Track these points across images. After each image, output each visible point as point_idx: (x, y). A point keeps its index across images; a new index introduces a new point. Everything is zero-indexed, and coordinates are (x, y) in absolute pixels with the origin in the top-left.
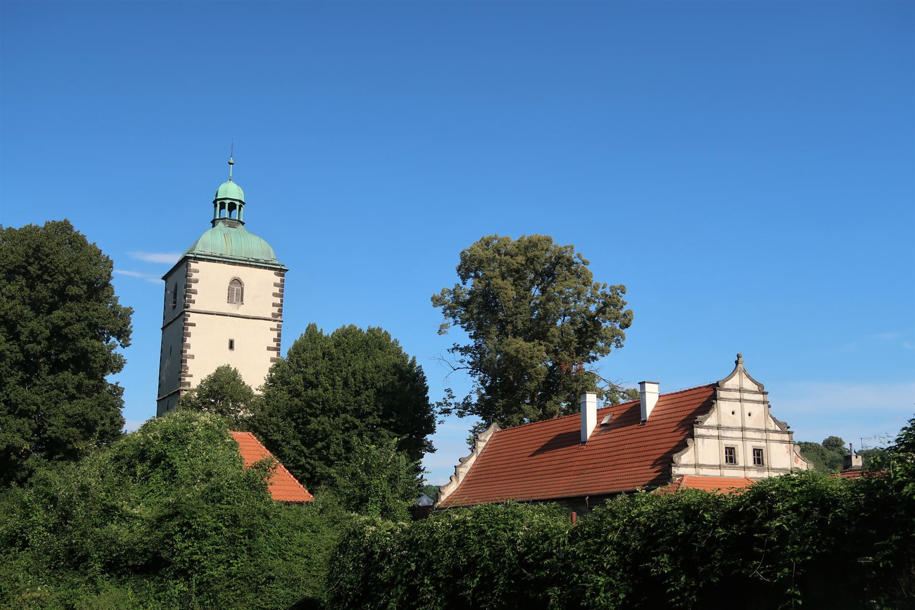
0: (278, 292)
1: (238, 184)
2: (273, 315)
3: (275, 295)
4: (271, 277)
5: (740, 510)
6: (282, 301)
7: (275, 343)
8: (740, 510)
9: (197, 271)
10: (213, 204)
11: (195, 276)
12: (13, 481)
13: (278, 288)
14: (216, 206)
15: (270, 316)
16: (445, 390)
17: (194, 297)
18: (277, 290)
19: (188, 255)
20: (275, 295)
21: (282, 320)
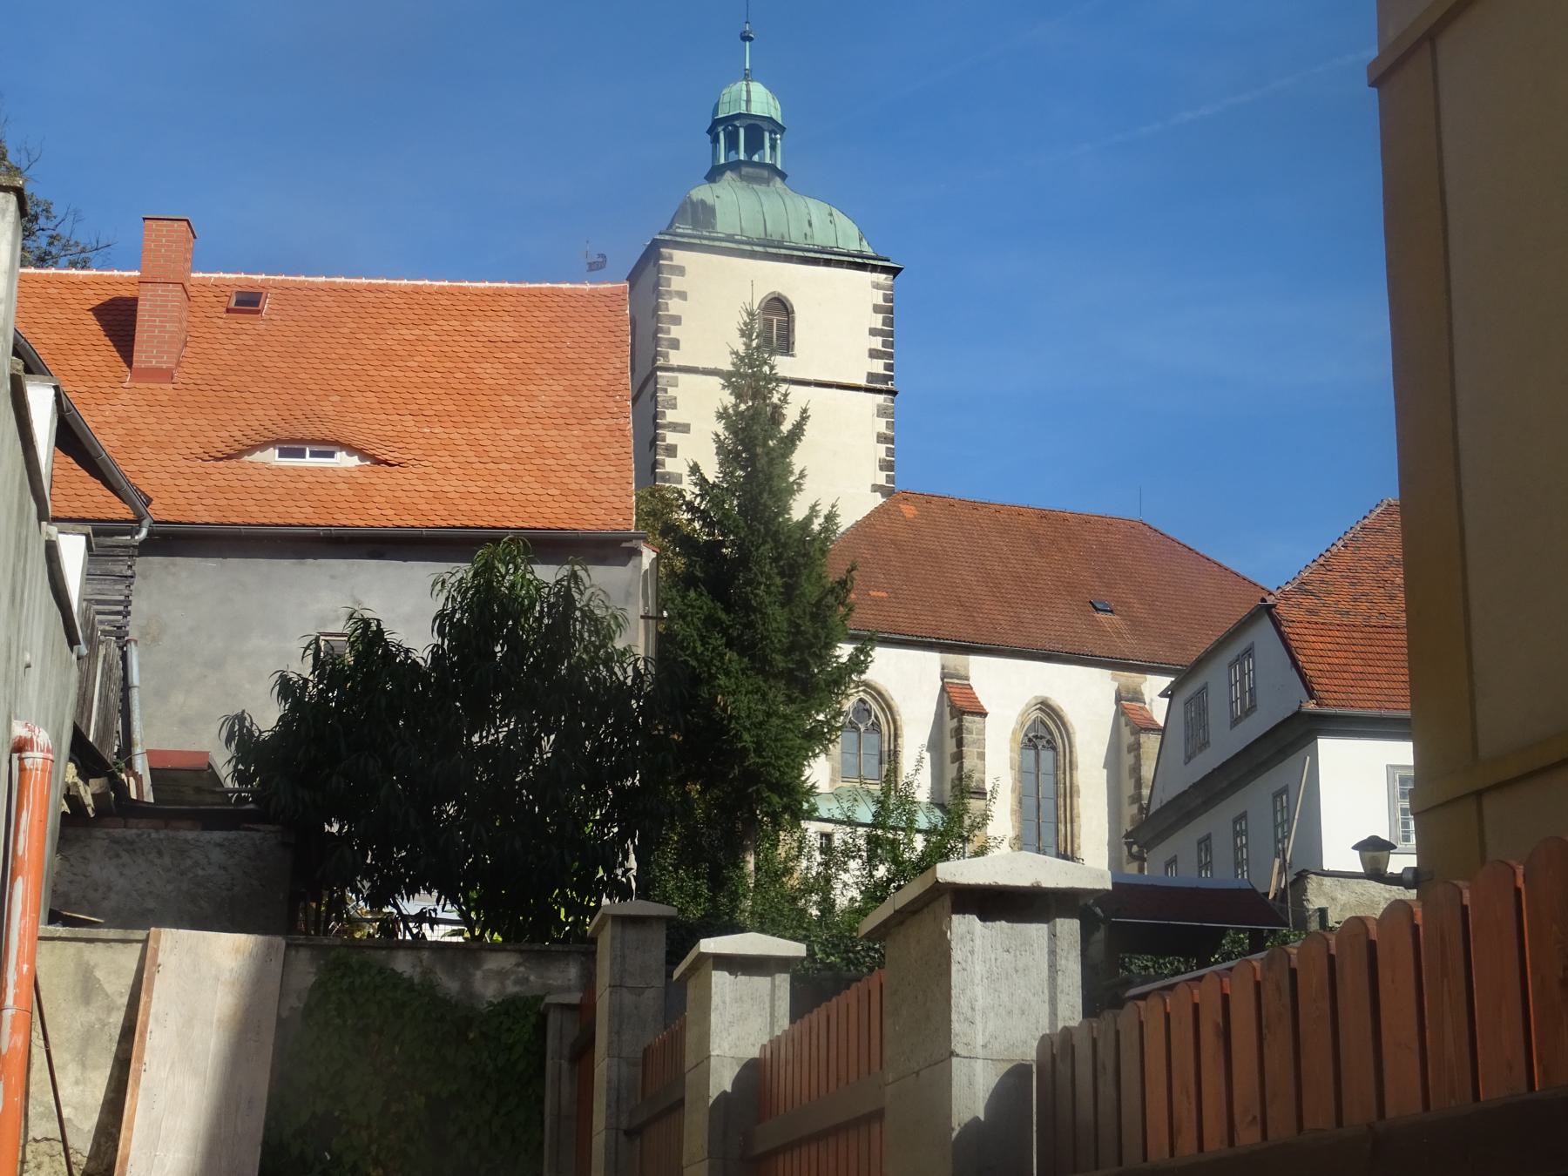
0: (879, 326)
1: (766, 86)
2: (872, 377)
3: (874, 354)
4: (864, 289)
5: (557, 891)
6: (889, 367)
7: (884, 421)
8: (557, 891)
9: (680, 271)
10: (709, 137)
11: (676, 283)
12: (816, 916)
13: (880, 339)
14: (715, 140)
15: (863, 382)
16: (1186, 764)
17: (675, 332)
18: (877, 343)
19: (658, 237)
20: (874, 354)
21: (894, 388)
